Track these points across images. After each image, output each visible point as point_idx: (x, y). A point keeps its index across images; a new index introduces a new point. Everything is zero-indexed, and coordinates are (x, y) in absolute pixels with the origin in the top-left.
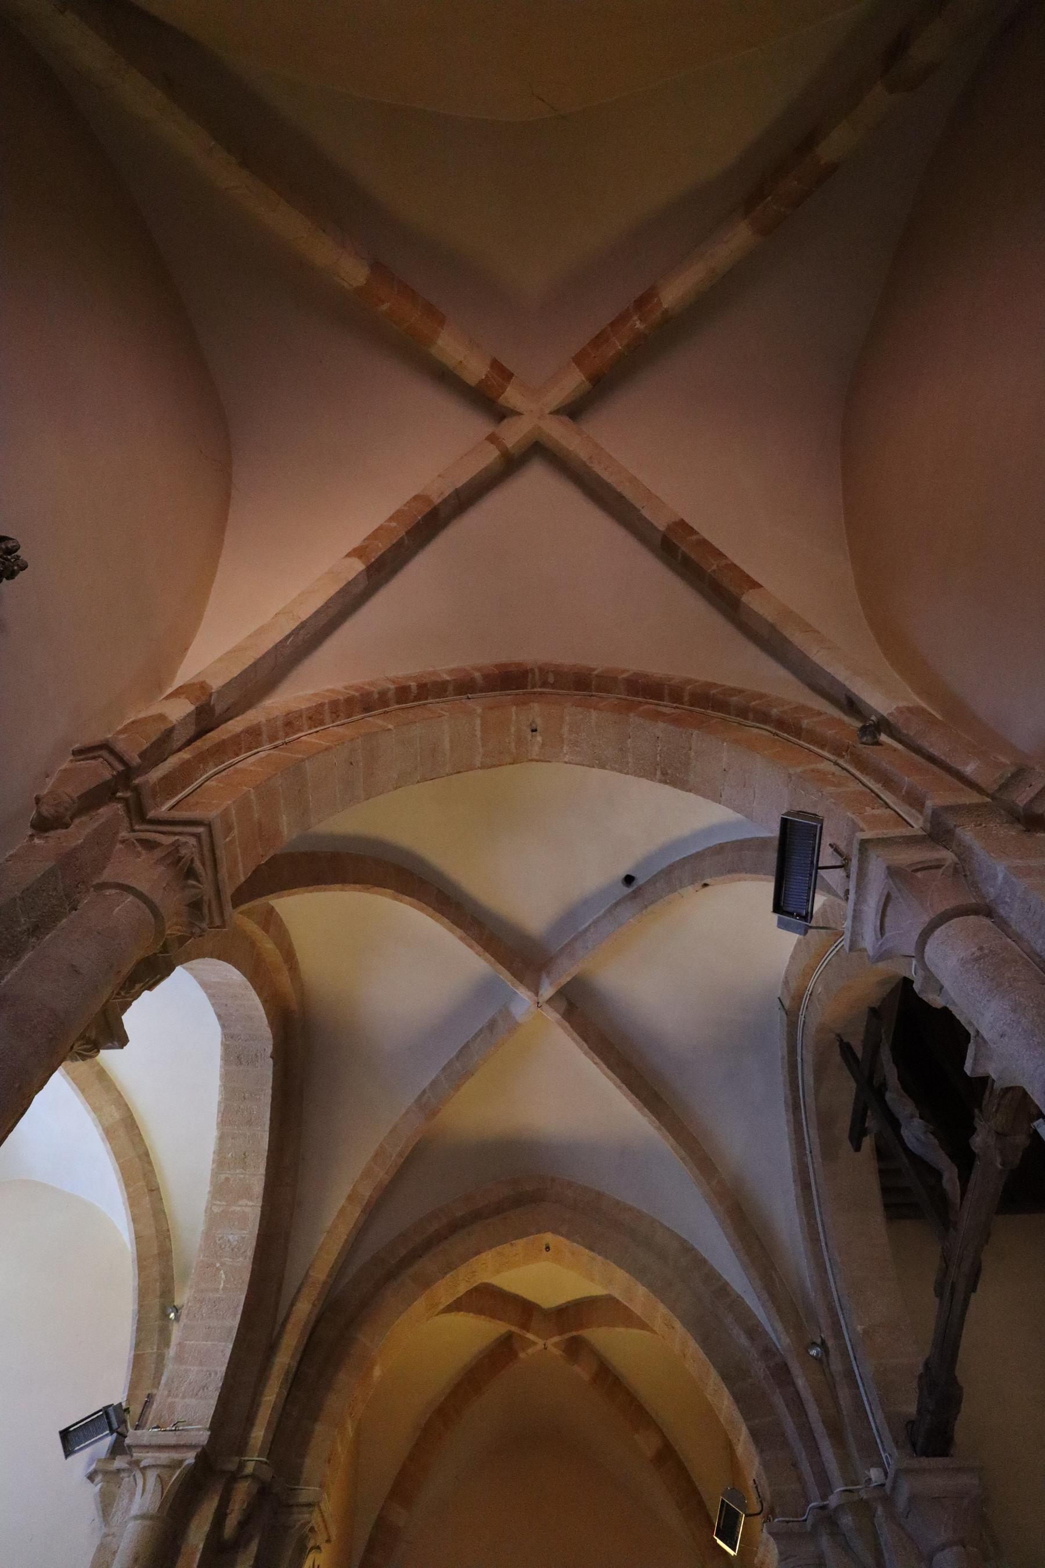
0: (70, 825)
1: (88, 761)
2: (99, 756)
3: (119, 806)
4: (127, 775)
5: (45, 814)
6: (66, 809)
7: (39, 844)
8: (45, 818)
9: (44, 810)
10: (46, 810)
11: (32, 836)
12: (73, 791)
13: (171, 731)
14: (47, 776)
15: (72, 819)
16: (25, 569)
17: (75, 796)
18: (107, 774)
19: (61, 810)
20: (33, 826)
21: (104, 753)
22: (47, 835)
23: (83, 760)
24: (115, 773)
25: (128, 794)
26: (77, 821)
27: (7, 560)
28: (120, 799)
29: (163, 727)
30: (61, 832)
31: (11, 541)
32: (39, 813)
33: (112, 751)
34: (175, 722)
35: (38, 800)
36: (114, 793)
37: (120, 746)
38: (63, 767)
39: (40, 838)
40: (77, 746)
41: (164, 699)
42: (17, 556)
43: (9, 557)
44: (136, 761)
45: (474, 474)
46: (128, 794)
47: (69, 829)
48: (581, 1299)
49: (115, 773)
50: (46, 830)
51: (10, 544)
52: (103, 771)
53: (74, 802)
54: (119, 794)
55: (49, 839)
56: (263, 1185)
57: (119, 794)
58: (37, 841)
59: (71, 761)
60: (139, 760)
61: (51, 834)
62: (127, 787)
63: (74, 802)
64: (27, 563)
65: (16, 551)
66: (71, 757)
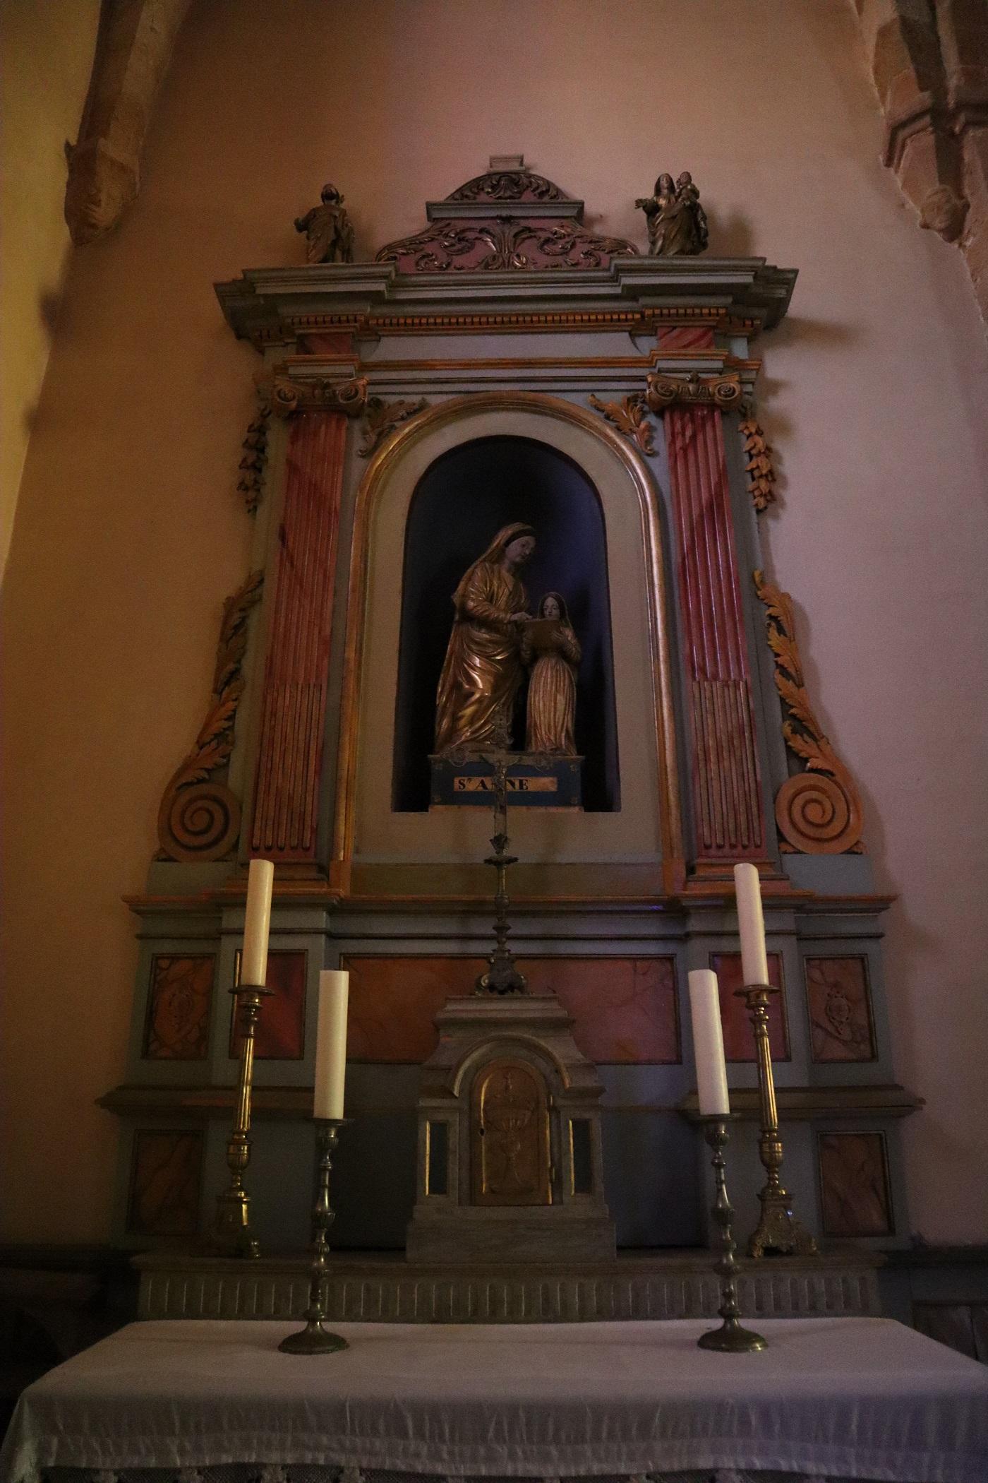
0: (967, 201)
1: (904, 155)
2: (904, 140)
3: (971, 133)
4: (938, 115)
5: (943, 225)
6: (948, 201)
7: (972, 243)
8: (947, 228)
9: (939, 225)
10: (940, 222)
11: (960, 245)
12: (931, 187)
13: (904, 21)
14: (903, 205)
15: (961, 197)
16: (690, 177)
17: (937, 186)
18: (928, 139)
19: (947, 207)
20: (951, 240)
21: (901, 135)
22: (966, 231)
23: (900, 159)
24: (931, 129)
25: (962, 118)
26: (967, 191)
27: (680, 194)
28: (964, 131)
29: (897, 36)
30: (970, 216)
31: (661, 182)
32: (940, 231)
33: (903, 125)
34: (895, 15)
35: (925, 226)
36: (952, 135)
37: (902, 113)
38: (900, 184)
39: (967, 239)
40: (881, 158)
41: (860, 14)
42: (677, 182)
43: (678, 190)
44: (925, 98)
45: (397, 645)
46: (962, 118)
47: (971, 204)
48: (695, 1033)
49: (931, 129)
50: (961, 231)
51: (664, 183)
52: (923, 142)
53: (944, 190)
54: (957, 129)
55: (972, 231)
56: (48, 1374)
57: (957, 129)
58: (968, 243)
59: (896, 172)
60: (927, 94)
61: (967, 225)
62: (953, 116)
63: (944, 190)
64: (684, 173)
65: (671, 180)
66: (892, 170)
